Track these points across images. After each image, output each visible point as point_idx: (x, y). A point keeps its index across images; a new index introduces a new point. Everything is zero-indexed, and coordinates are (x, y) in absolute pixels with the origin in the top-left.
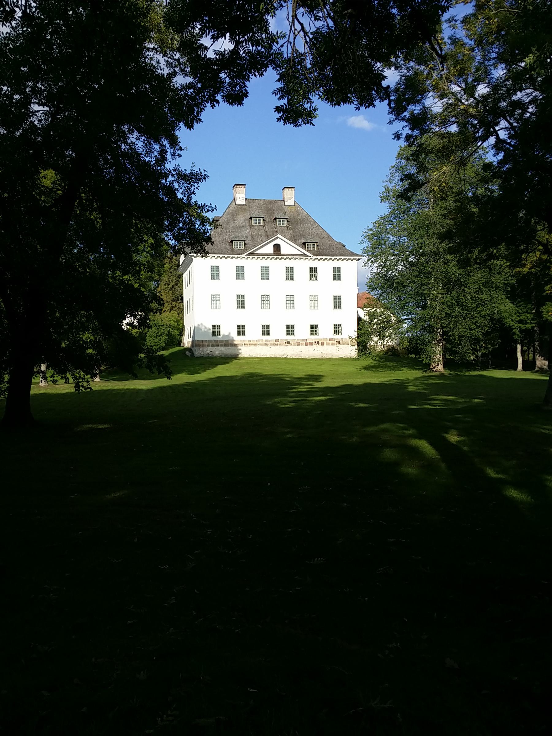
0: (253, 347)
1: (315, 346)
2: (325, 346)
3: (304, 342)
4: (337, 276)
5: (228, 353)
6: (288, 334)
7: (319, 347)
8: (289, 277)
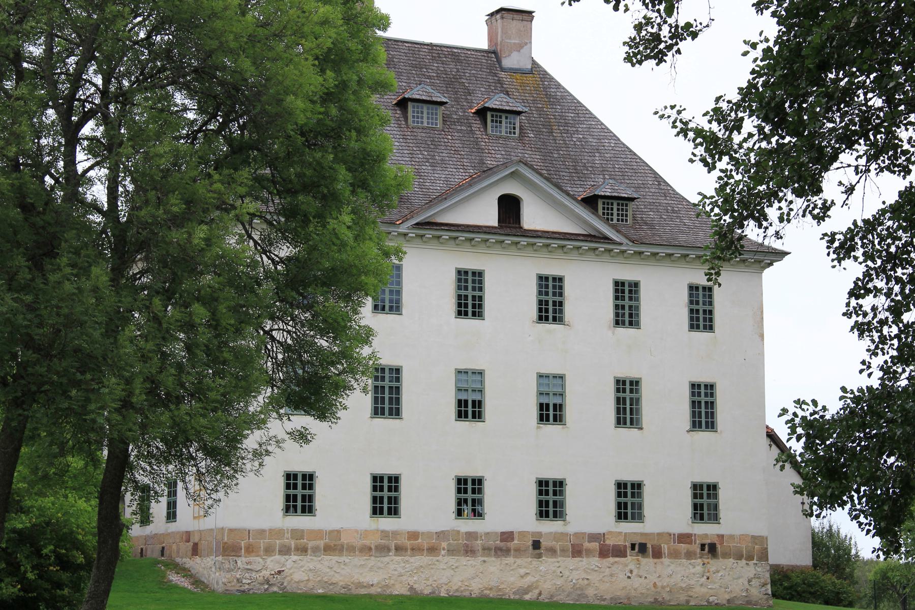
0: (422, 560)
1: (631, 560)
2: (666, 561)
3: (595, 545)
4: (701, 316)
5: (336, 578)
6: (377, 511)
7: (647, 562)
8: (466, 306)
